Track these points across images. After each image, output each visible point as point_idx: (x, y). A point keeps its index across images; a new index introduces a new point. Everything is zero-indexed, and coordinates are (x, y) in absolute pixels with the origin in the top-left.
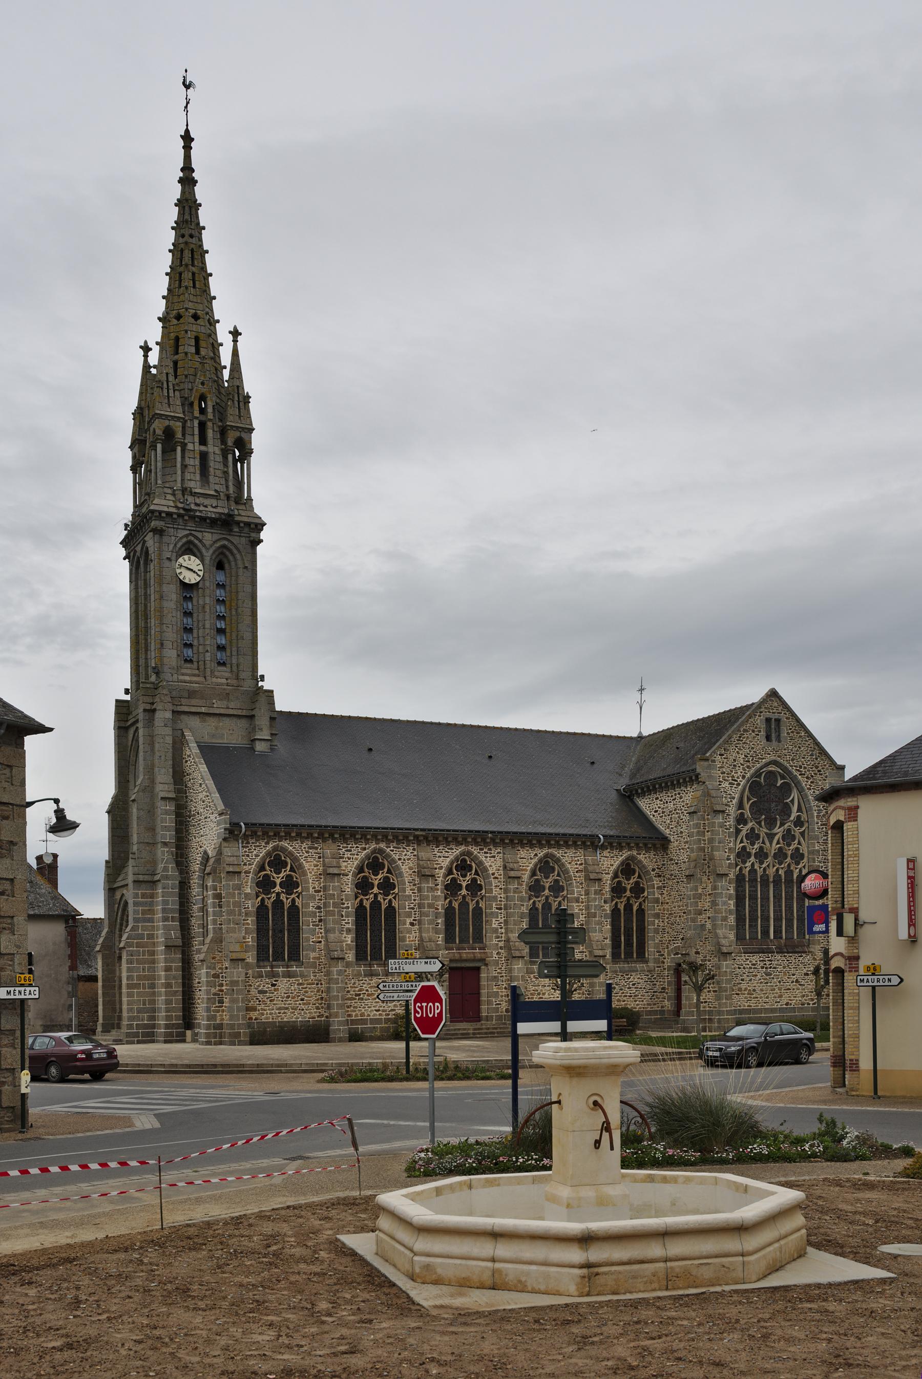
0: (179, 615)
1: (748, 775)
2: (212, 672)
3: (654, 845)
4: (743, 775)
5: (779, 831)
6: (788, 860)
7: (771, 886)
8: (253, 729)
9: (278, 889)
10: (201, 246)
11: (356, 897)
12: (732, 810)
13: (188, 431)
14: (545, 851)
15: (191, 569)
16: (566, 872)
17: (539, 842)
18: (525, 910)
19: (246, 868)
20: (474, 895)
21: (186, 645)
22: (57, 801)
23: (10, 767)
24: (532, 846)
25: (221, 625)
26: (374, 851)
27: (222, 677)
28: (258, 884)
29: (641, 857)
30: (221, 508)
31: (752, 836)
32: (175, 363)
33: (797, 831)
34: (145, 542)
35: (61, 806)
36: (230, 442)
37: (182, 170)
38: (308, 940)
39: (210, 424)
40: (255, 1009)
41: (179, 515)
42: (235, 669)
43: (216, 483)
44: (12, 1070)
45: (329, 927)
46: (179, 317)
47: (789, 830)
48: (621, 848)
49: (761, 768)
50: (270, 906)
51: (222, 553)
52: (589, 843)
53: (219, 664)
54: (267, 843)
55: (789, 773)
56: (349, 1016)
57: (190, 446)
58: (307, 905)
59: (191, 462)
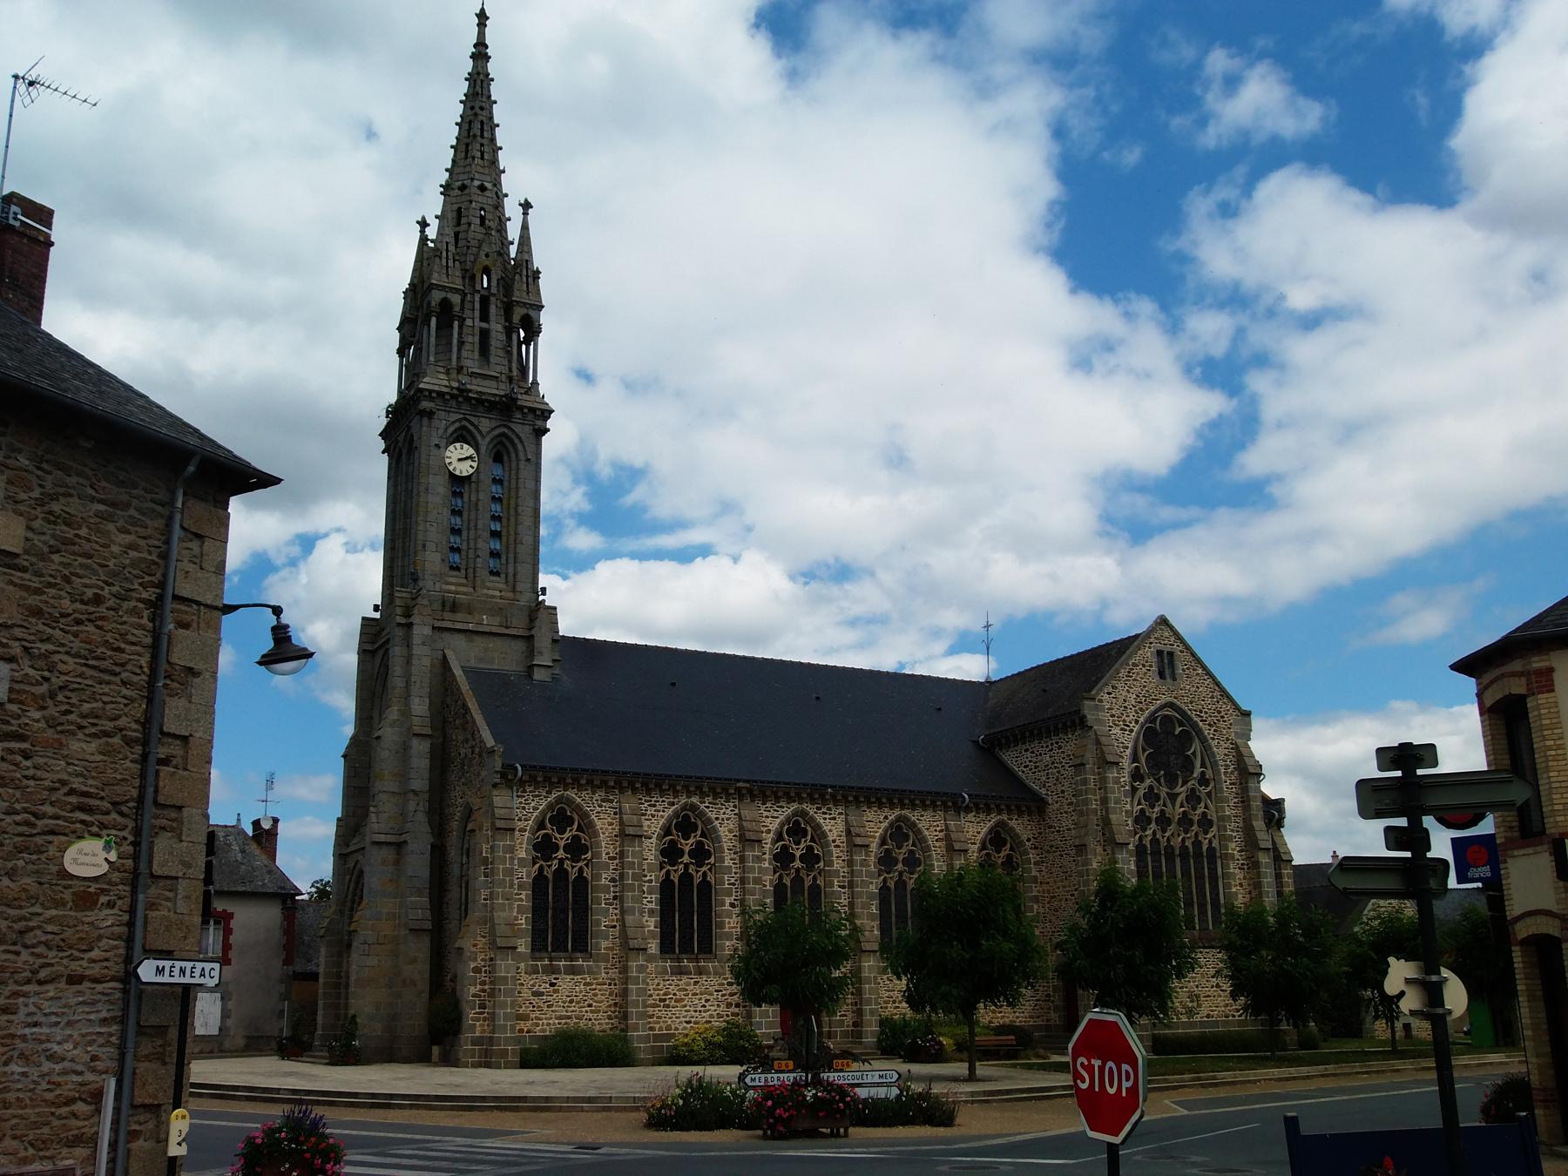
0: (446, 512)
1: (1142, 720)
2: (483, 582)
3: (1028, 808)
4: (1135, 720)
5: (1181, 790)
6: (1195, 827)
7: (1178, 860)
8: (531, 652)
9: (561, 854)
10: (491, 118)
11: (662, 868)
12: (1126, 763)
13: (467, 305)
14: (897, 812)
15: (460, 459)
16: (923, 840)
17: (890, 801)
18: (873, 889)
19: (521, 824)
20: (810, 868)
21: (452, 549)
22: (277, 611)
23: (200, 537)
24: (881, 806)
25: (496, 526)
26: (684, 808)
27: (494, 589)
28: (536, 847)
29: (1013, 823)
30: (501, 389)
31: (1152, 797)
32: (457, 235)
33: (1203, 790)
34: (409, 428)
35: (285, 619)
36: (516, 318)
37: (475, 46)
38: (598, 923)
39: (493, 299)
40: (524, 1018)
41: (453, 396)
42: (511, 578)
43: (497, 365)
44: (154, 1109)
45: (629, 904)
46: (463, 188)
47: (1193, 790)
48: (988, 811)
49: (1156, 711)
50: (550, 876)
51: (501, 443)
52: (952, 804)
53: (492, 573)
54: (549, 792)
55: (1189, 719)
56: (652, 1029)
57: (469, 322)
58: (598, 877)
59: (470, 339)
